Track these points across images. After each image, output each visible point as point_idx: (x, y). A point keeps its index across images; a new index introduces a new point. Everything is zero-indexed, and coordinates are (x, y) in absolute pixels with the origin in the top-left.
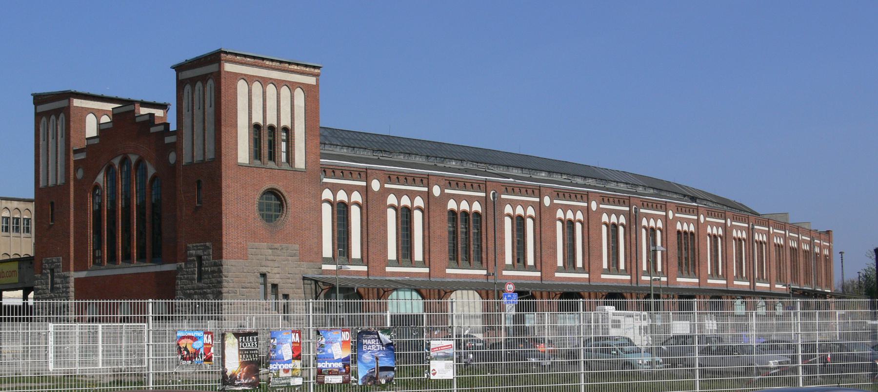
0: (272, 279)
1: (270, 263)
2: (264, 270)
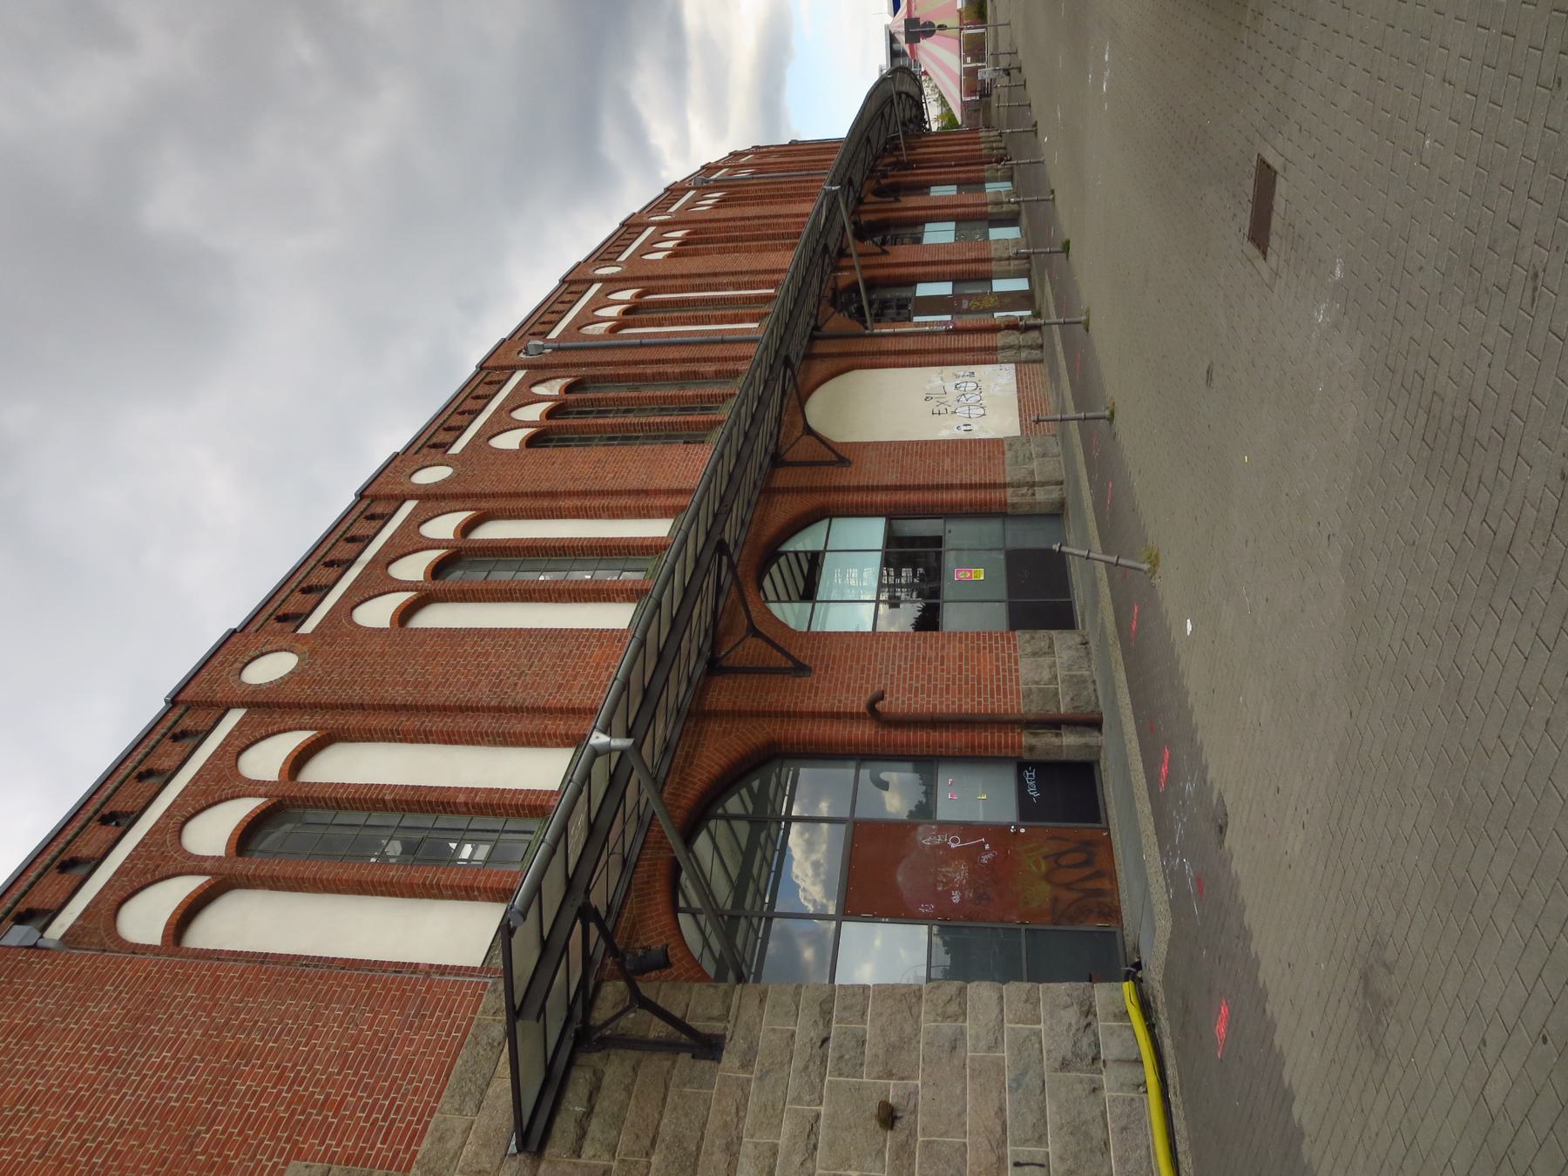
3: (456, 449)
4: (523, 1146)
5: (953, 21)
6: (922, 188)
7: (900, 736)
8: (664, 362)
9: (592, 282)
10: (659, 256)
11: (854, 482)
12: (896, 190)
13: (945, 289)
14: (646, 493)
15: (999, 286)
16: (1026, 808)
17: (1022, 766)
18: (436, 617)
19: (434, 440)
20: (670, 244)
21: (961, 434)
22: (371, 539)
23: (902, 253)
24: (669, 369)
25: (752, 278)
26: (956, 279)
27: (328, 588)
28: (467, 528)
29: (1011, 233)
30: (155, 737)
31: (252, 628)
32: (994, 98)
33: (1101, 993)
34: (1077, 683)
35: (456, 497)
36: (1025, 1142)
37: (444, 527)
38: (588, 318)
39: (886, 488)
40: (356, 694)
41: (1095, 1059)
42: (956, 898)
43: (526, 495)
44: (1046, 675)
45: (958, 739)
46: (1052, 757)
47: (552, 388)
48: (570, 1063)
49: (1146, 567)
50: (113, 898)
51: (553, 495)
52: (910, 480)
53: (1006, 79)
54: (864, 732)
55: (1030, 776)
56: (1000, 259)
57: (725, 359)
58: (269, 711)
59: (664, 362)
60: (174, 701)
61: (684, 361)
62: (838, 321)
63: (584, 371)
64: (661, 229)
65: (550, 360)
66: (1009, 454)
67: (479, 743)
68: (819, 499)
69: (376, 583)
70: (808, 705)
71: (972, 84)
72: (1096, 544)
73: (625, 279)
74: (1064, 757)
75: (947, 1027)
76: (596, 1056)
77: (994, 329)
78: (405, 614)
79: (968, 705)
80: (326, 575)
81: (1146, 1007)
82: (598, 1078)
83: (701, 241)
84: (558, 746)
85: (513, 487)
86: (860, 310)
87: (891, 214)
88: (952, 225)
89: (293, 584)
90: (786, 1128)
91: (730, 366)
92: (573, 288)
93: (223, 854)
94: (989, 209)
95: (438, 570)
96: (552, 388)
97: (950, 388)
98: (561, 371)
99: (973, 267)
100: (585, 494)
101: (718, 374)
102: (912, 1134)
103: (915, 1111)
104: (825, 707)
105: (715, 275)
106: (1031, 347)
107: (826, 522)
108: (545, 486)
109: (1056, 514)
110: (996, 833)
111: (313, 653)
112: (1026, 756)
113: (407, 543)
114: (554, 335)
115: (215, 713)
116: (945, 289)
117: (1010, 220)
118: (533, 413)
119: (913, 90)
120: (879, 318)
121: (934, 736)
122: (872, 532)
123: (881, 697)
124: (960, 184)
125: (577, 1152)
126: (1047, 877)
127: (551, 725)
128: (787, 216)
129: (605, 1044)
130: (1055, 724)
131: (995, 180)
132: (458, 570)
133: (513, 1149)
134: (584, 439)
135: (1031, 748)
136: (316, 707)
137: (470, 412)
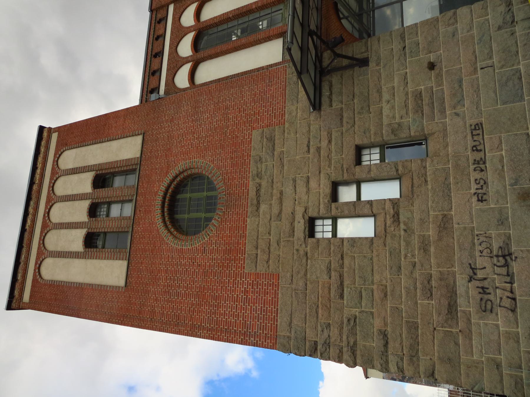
4: (314, 109)
31: (144, 102)
36: (484, 60)
69: (176, 63)
76: (328, 77)
90: (396, 80)
95: (196, 45)
102: (441, 69)
103: (441, 62)
125: (331, 106)
133: (312, 110)
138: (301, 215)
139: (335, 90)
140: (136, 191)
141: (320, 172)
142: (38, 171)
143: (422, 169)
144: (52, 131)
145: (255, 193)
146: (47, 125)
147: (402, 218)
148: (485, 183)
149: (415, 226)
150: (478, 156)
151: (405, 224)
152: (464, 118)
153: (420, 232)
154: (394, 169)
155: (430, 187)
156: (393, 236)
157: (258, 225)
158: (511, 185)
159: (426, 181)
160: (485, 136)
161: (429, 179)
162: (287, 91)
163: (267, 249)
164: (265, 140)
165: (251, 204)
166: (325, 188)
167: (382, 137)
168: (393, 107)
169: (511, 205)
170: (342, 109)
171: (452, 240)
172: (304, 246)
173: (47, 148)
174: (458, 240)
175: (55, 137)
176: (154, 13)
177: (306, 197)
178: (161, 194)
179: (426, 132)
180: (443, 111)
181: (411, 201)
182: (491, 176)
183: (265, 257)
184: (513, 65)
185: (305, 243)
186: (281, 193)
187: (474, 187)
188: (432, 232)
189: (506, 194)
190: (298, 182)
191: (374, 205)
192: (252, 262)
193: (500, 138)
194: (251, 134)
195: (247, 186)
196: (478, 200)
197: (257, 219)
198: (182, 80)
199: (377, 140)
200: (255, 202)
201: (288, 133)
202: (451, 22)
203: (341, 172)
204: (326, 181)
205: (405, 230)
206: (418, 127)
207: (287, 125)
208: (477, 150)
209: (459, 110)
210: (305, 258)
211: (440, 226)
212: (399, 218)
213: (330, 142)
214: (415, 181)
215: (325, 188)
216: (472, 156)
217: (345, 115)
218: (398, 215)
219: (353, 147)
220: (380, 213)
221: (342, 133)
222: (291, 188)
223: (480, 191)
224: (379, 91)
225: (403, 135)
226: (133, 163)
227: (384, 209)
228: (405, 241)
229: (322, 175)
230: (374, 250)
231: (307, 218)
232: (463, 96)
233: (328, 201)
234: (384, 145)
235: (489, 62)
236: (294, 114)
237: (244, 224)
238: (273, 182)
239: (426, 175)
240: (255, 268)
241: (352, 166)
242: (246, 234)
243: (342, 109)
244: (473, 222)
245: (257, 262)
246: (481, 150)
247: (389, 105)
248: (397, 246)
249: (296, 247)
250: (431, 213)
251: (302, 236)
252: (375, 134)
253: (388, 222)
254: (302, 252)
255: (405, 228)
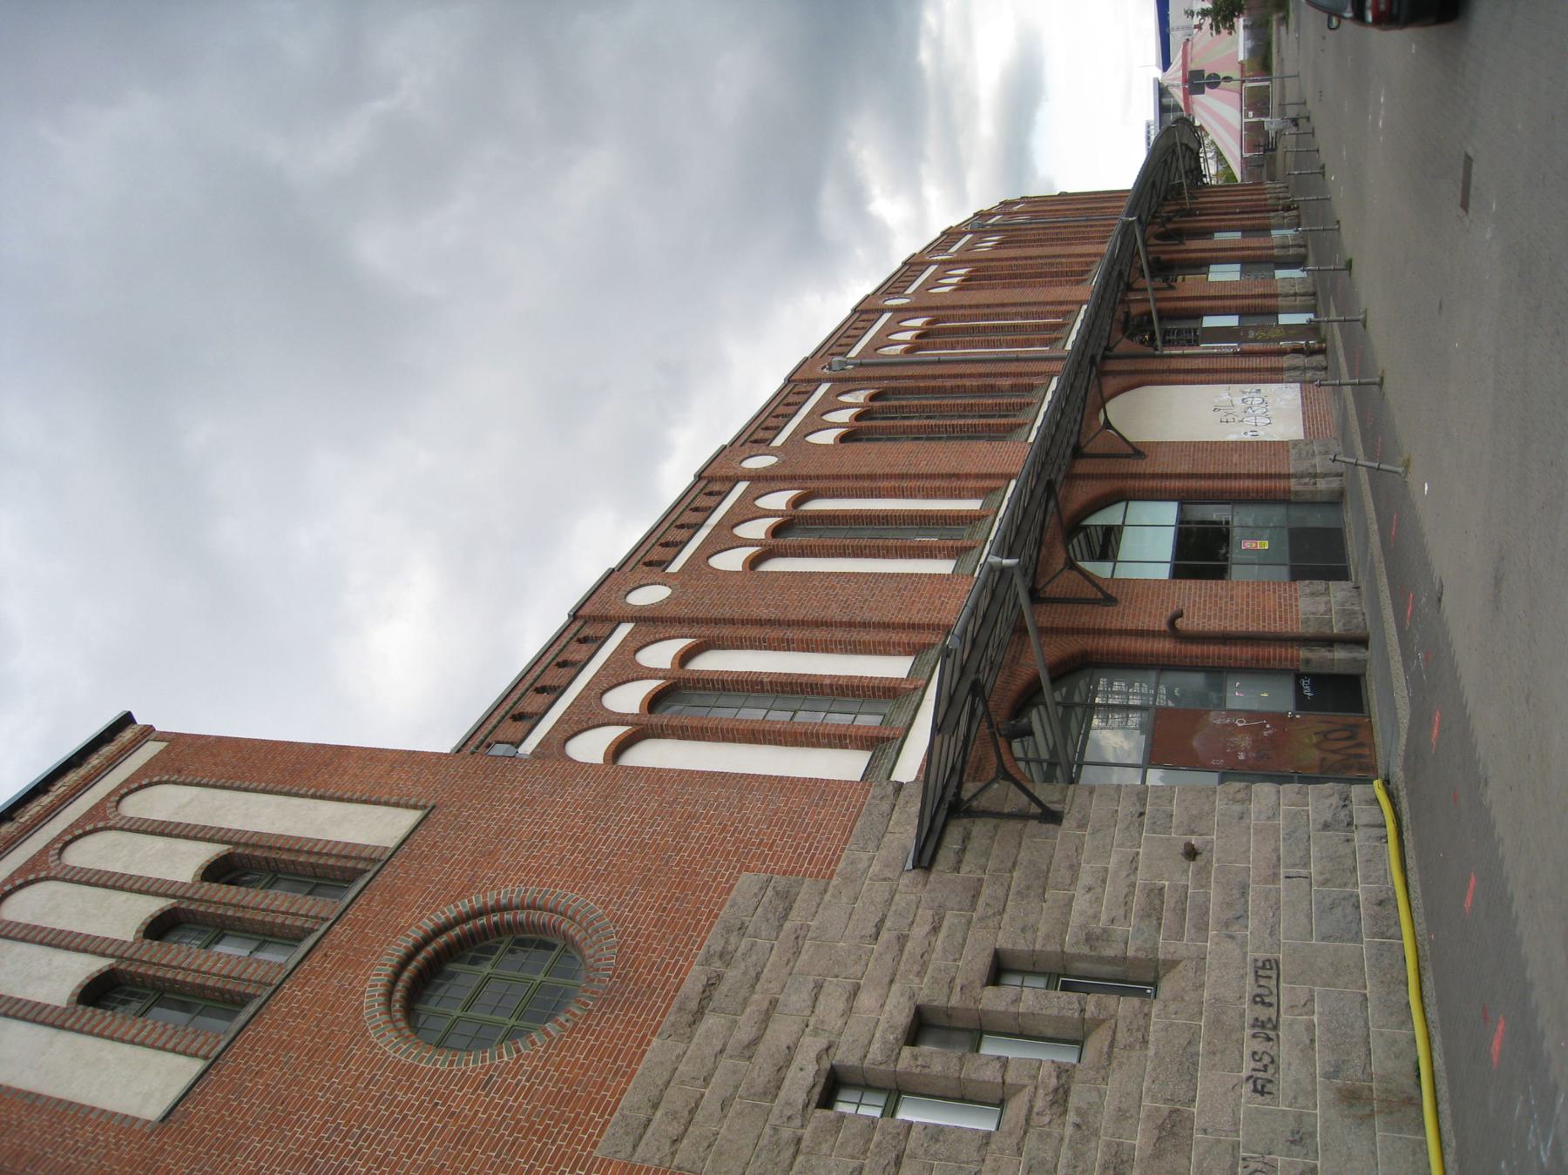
0: (870, 1028)
1: (781, 1031)
2: (803, 1077)
3: (675, 567)
4: (917, 864)
5: (1235, 74)
6: (1207, 233)
7: (1195, 649)
8: (962, 376)
9: (882, 311)
10: (946, 289)
11: (1149, 470)
12: (1179, 235)
13: (1232, 321)
14: (958, 476)
15: (1284, 319)
16: (1301, 703)
17: (1299, 677)
18: (652, 755)
19: (755, 437)
20: (955, 280)
21: (1249, 438)
22: (541, 716)
23: (1188, 284)
24: (967, 382)
25: (1041, 309)
26: (1242, 313)
27: (683, 544)
28: (685, 657)
29: (1296, 273)
30: (564, 640)
31: (467, 751)
32: (1279, 152)
33: (1356, 791)
34: (1348, 614)
35: (784, 478)
36: (1294, 866)
37: (660, 655)
38: (883, 340)
39: (1179, 476)
40: (726, 612)
41: (1350, 824)
42: (1242, 757)
43: (848, 477)
44: (1322, 608)
45: (1244, 653)
46: (1325, 670)
47: (859, 397)
48: (945, 826)
49: (1400, 470)
50: (560, 736)
51: (871, 477)
52: (1201, 470)
53: (1294, 130)
54: (1165, 646)
55: (1306, 686)
56: (1287, 295)
57: (1020, 375)
58: (653, 624)
59: (962, 376)
60: (575, 616)
61: (981, 375)
62: (1124, 345)
63: (885, 383)
64: (944, 268)
65: (853, 374)
66: (1293, 452)
67: (832, 651)
68: (1117, 484)
69: (589, 715)
70: (1116, 624)
71: (1259, 143)
72: (1360, 451)
73: (915, 309)
74: (1335, 671)
75: (1237, 808)
76: (965, 821)
77: (1282, 353)
78: (619, 749)
79: (1254, 627)
80: (537, 701)
81: (1391, 796)
82: (966, 839)
83: (985, 278)
84: (900, 654)
85: (835, 471)
86: (1152, 335)
87: (1176, 256)
88: (1237, 267)
89: (638, 556)
90: (1114, 859)
91: (1026, 380)
92: (865, 317)
93: (668, 666)
94: (1275, 252)
95: (655, 702)
96: (859, 397)
97: (1237, 401)
98: (865, 384)
99: (1259, 301)
100: (902, 477)
101: (1013, 387)
102: (1209, 862)
103: (1211, 851)
104: (1131, 626)
105: (1003, 305)
106: (1316, 369)
107: (1123, 504)
108: (865, 470)
109: (1336, 501)
110: (1278, 718)
111: (683, 585)
112: (1303, 669)
113: (623, 670)
114: (853, 354)
115: (609, 626)
116: (1232, 321)
117: (1298, 262)
118: (844, 416)
119: (1194, 145)
120: (1166, 343)
121: (1225, 650)
122: (1168, 512)
123: (1180, 615)
124: (1245, 231)
125: (958, 870)
126: (1317, 746)
127: (894, 637)
128: (1070, 256)
129: (971, 814)
130: (1329, 642)
131: (1280, 227)
132: (677, 704)
133: (909, 865)
134: (891, 436)
135: (1308, 661)
136: (694, 621)
137: (784, 416)
138: (813, 1055)
139: (974, 845)
140: (337, 913)
141: (892, 981)
142: (46, 800)
143: (1141, 1016)
144: (153, 735)
145: (700, 987)
146: (141, 720)
147: (1074, 1101)
148: (1272, 1062)
149: (1105, 1122)
150: (1264, 1013)
151: (1079, 1112)
152: (1243, 945)
153: (1113, 1135)
154: (1076, 1006)
155: (1151, 1052)
156: (1044, 1137)
157: (679, 1058)
158: (1327, 1076)
159: (1145, 1042)
160: (1282, 985)
161: (1151, 1038)
162: (858, 824)
163: (686, 1113)
164: (770, 892)
165: (680, 1009)
166: (895, 1013)
167: (1062, 945)
168: (1098, 900)
169: (1322, 1113)
170: (980, 880)
171: (1185, 1161)
172: (797, 1122)
173: (113, 763)
174: (1200, 1163)
175: (151, 749)
176: (578, 624)
177: (840, 1022)
178: (416, 934)
179: (1161, 956)
180: (1202, 928)
181: (1103, 1072)
182: (1285, 1052)
183: (675, 1129)
184: (1345, 885)
185: (803, 1116)
186: (774, 1003)
187: (1248, 1066)
188: (1140, 1140)
189: (1315, 1090)
190: (828, 988)
191: (1011, 1067)
192: (627, 1134)
193: (1311, 992)
194: (736, 879)
195: (681, 973)
196: (1255, 1091)
197: (683, 1046)
198: (590, 747)
199: (1049, 949)
200: (693, 1005)
201: (833, 896)
202: (1239, 796)
203: (946, 990)
204: (904, 1000)
205: (1078, 1126)
206: (1145, 941)
207: (835, 881)
208: (1263, 1003)
209: (1234, 928)
210: (792, 1149)
211: (1161, 1127)
212: (1066, 1101)
213: (935, 930)
214: (1119, 1035)
215: (895, 1013)
216: (1250, 1012)
217: (986, 891)
218: (1067, 1093)
219: (989, 952)
220: (1025, 1086)
221: (969, 922)
222: (805, 995)
223: (1260, 1074)
224: (1074, 869)
225: (1109, 952)
226: (365, 854)
227: (1035, 1077)
228: (1070, 1147)
229: (895, 987)
230: (988, 1157)
231: (826, 1065)
232: (1246, 911)
233: (897, 1039)
234: (1059, 976)
235: (1303, 872)
236: (862, 866)
237: (639, 1046)
238: (758, 977)
239: (1147, 1028)
240: (629, 1149)
241: (978, 984)
242: (634, 1071)
243: (980, 880)
244: (1237, 1131)
245: (641, 1137)
246: (1270, 1005)
247: (1088, 896)
248: (1049, 1156)
249: (772, 1120)
250: (1146, 1102)
251: (801, 1098)
252: (1047, 937)
253: (1039, 1104)
254: (787, 1133)
255: (1078, 1120)
